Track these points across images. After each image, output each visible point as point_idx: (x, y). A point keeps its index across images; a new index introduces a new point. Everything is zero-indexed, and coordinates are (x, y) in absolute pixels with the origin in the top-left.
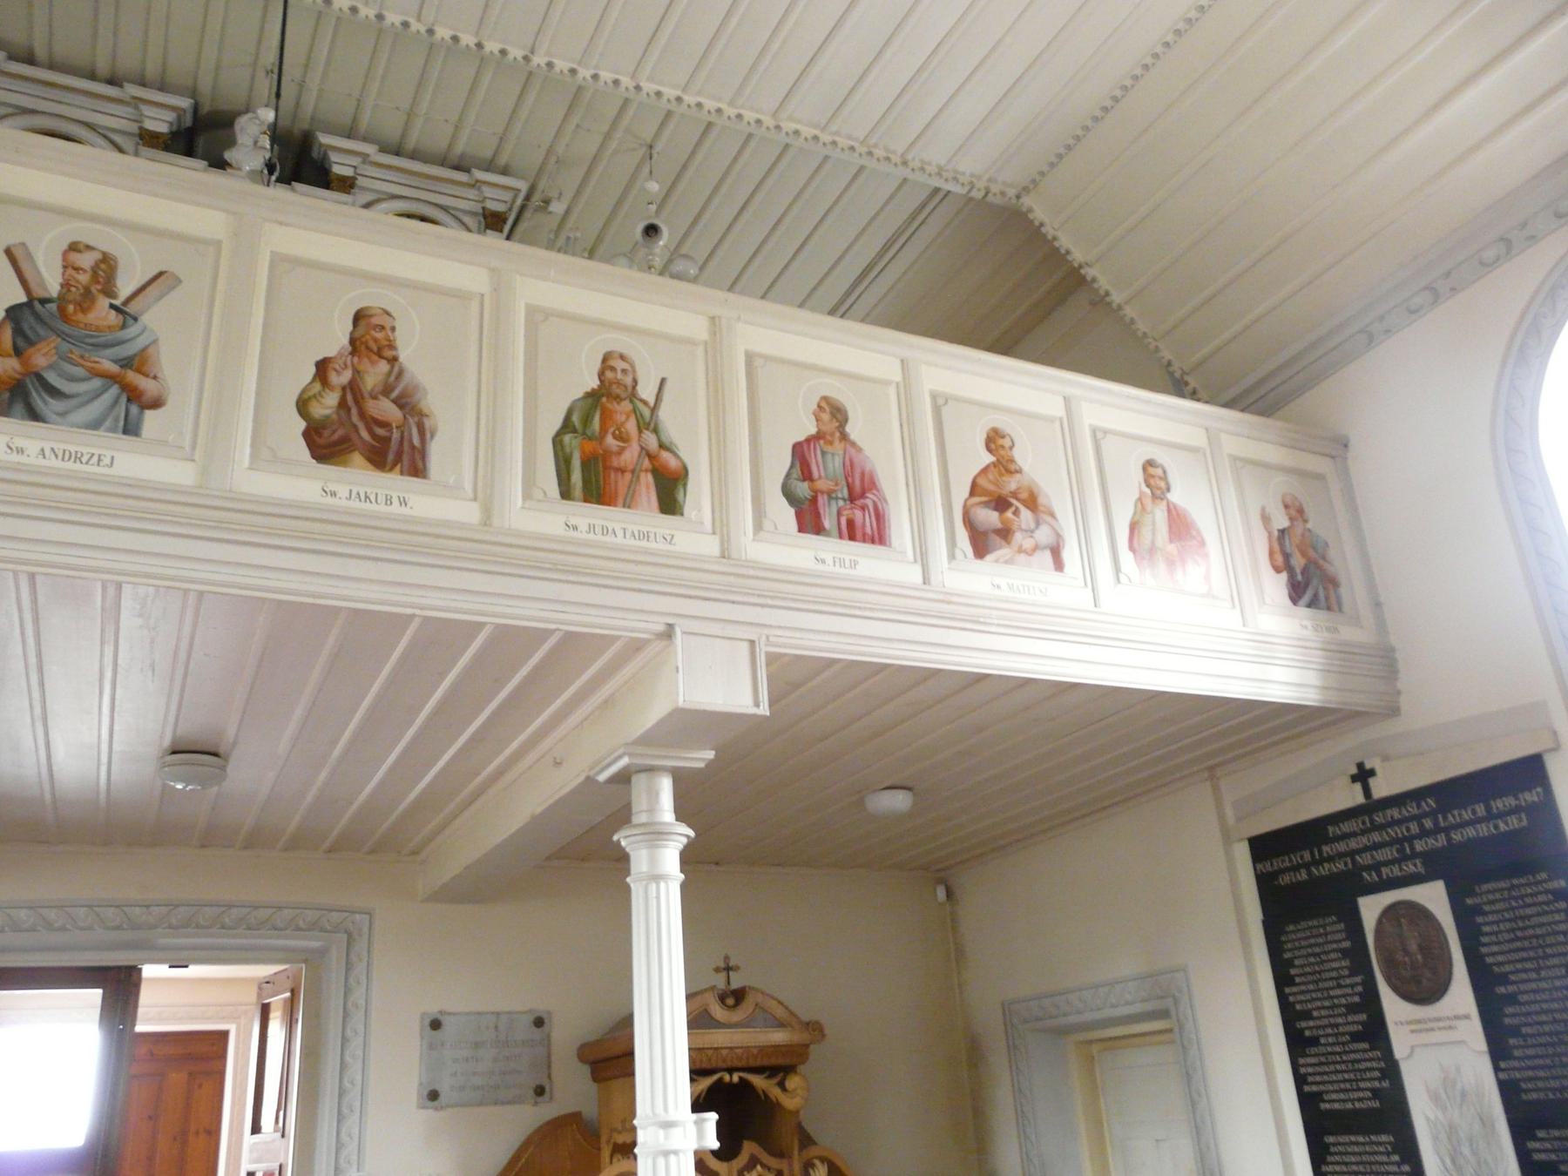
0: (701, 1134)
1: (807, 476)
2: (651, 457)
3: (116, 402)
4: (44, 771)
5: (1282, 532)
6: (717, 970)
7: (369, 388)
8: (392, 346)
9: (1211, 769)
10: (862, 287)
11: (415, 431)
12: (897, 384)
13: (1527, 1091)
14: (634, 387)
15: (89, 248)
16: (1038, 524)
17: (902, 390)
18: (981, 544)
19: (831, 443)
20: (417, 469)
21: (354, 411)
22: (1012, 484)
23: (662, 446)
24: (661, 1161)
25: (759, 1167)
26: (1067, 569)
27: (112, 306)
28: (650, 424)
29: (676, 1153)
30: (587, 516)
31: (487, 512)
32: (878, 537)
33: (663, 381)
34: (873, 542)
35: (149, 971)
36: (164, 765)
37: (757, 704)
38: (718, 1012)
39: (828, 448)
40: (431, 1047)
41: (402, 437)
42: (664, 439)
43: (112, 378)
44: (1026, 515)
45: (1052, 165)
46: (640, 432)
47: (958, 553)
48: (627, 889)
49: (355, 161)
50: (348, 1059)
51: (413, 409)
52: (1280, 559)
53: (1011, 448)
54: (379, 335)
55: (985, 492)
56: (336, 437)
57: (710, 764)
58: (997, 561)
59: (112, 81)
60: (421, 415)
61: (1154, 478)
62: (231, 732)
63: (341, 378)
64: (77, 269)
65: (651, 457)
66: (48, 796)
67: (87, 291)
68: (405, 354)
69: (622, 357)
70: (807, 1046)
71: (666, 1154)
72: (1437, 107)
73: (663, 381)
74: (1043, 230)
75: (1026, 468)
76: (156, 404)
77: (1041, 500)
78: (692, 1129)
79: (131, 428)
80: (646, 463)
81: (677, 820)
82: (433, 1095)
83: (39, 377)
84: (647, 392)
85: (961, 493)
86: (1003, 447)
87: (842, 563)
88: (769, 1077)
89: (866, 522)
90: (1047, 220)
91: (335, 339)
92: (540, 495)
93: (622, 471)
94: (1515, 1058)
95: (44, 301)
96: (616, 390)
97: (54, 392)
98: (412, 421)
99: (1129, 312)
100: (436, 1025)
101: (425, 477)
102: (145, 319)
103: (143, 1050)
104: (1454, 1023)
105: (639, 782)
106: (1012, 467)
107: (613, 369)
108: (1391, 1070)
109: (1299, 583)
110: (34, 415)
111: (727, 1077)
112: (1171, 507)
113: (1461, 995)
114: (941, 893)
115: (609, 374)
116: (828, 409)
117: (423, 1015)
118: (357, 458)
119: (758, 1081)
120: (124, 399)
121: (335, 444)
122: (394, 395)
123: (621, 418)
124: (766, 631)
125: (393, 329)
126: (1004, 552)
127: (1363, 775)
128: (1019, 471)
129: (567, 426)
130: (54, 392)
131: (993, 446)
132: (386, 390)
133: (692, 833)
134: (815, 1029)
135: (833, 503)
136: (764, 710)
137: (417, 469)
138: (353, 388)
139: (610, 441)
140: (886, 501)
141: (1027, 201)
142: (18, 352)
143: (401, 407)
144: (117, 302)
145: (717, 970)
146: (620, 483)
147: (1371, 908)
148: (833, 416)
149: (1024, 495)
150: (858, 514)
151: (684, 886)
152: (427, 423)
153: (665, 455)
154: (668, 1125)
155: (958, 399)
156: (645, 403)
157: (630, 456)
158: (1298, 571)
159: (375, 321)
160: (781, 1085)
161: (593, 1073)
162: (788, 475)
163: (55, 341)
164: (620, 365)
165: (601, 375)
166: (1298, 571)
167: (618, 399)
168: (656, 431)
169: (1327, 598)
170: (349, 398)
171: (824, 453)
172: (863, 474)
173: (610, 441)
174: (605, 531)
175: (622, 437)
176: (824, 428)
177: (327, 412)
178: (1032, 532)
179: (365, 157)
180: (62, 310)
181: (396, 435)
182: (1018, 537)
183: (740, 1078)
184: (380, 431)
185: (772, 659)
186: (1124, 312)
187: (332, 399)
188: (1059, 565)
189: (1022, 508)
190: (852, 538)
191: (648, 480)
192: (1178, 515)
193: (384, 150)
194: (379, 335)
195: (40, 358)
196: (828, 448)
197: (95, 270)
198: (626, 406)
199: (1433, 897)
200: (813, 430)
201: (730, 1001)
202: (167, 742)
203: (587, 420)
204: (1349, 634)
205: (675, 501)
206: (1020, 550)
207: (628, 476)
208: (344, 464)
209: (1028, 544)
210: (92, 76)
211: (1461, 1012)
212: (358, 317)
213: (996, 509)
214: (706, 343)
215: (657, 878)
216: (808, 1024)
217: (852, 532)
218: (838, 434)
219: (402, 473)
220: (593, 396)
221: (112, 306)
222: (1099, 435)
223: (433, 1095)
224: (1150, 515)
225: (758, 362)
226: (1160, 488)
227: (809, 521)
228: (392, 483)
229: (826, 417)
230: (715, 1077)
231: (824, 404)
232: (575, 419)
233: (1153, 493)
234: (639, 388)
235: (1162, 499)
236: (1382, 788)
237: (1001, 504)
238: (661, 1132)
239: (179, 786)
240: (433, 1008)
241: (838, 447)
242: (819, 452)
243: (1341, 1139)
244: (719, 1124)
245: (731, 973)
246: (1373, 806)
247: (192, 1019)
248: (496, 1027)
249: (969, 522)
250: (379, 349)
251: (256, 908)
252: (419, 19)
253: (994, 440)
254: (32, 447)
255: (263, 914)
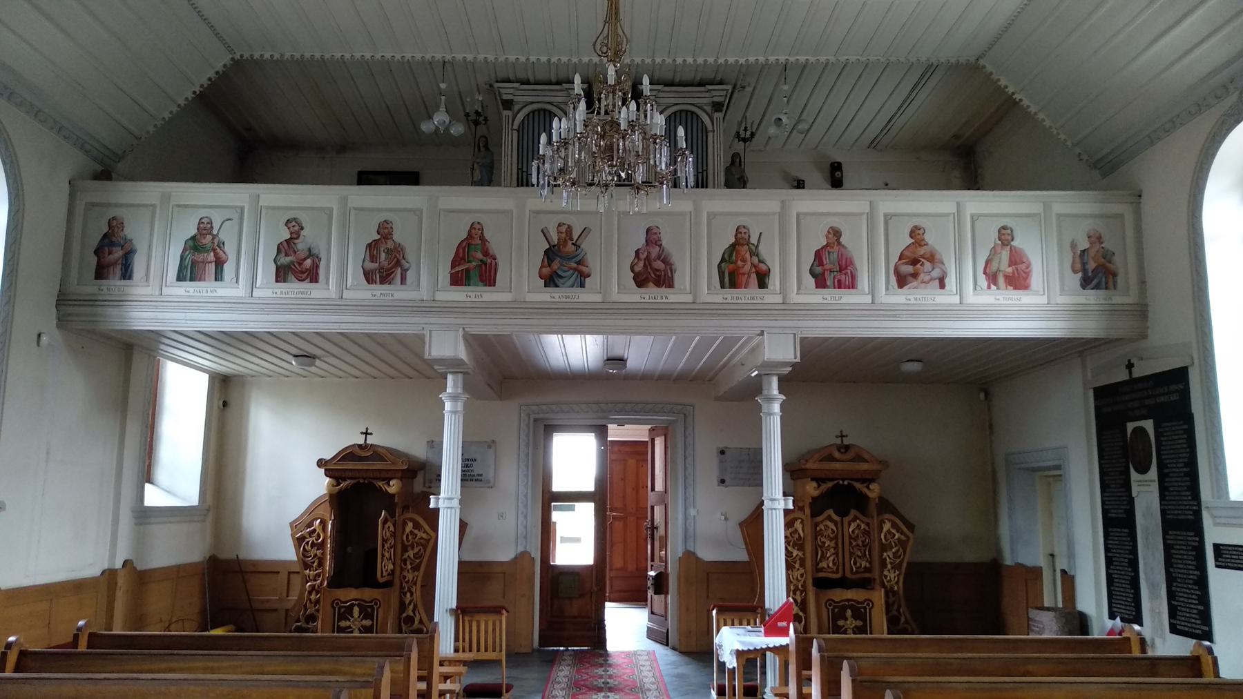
0: (786, 504)
1: (821, 264)
2: (755, 267)
3: (577, 276)
4: (567, 365)
5: (1083, 252)
6: (837, 437)
7: (653, 257)
8: (660, 240)
9: (1081, 352)
10: (917, 90)
11: (669, 271)
12: (867, 214)
13: (1169, 514)
14: (749, 239)
15: (564, 224)
16: (933, 269)
17: (869, 217)
18: (902, 281)
19: (833, 248)
20: (671, 286)
21: (649, 267)
22: (922, 251)
23: (760, 261)
24: (770, 511)
25: (858, 521)
26: (947, 287)
27: (573, 244)
28: (755, 253)
29: (775, 509)
30: (731, 295)
31: (695, 297)
32: (852, 285)
33: (761, 233)
34: (849, 288)
35: (609, 425)
36: (605, 365)
37: (795, 358)
38: (837, 455)
39: (832, 250)
40: (721, 462)
41: (665, 275)
42: (761, 258)
43: (575, 269)
44: (928, 265)
45: (989, 48)
46: (751, 257)
47: (890, 287)
48: (781, 411)
49: (511, 91)
50: (688, 465)
51: (668, 262)
52: (1078, 266)
53: (923, 234)
54: (655, 237)
55: (907, 258)
56: (643, 278)
57: (790, 372)
58: (909, 288)
59: (558, 83)
60: (671, 264)
61: (1005, 236)
62: (626, 357)
63: (643, 256)
64: (561, 233)
65: (755, 267)
66: (568, 370)
67: (565, 239)
68: (664, 243)
69: (744, 227)
70: (880, 471)
71: (772, 509)
72: (1155, 40)
73: (761, 233)
74: (992, 77)
75: (930, 242)
76: (589, 276)
77: (937, 256)
78: (782, 502)
79: (582, 285)
80: (754, 270)
81: (780, 393)
82: (723, 481)
83: (555, 272)
84: (754, 240)
85: (894, 259)
86: (919, 234)
87: (835, 299)
88: (862, 483)
89: (845, 279)
90: (994, 71)
91: (640, 241)
92: (713, 288)
93: (744, 274)
94: (1166, 500)
95: (554, 246)
96: (742, 241)
97: (561, 277)
98: (668, 268)
99: (1041, 116)
100: (722, 452)
101: (673, 287)
102: (582, 246)
103: (616, 448)
104: (1150, 483)
105: (765, 379)
106: (923, 243)
107: (475, 229)
108: (1131, 501)
109: (1089, 277)
110: (557, 286)
111: (841, 482)
112: (1013, 248)
113: (1153, 473)
114: (982, 396)
115: (739, 235)
116: (832, 233)
117: (718, 448)
118: (651, 284)
119: (857, 485)
120: (579, 276)
121: (643, 280)
122: (662, 258)
123: (743, 253)
124: (801, 329)
125: (660, 233)
126: (915, 284)
127: (1130, 366)
128: (927, 244)
129: (723, 260)
130: (561, 277)
131: (913, 235)
132: (659, 257)
133: (784, 398)
134: (885, 464)
135: (832, 274)
136: (798, 360)
137: (671, 286)
138: (648, 258)
139: (739, 263)
140: (856, 269)
141: (982, 62)
142: (549, 266)
143: (664, 263)
144: (574, 242)
145: (837, 437)
146: (743, 279)
147: (1130, 426)
148: (834, 235)
149: (928, 256)
150: (843, 277)
151: (781, 417)
152: (673, 267)
153: (761, 265)
154: (773, 500)
155: (896, 215)
156: (753, 244)
157: (748, 267)
158: (1090, 271)
159: (654, 231)
160: (868, 487)
161: (791, 476)
162: (812, 265)
163: (559, 259)
164: (743, 230)
165: (736, 236)
166: (1090, 271)
167: (743, 245)
168: (757, 256)
169: (1106, 283)
170: (647, 262)
171: (829, 252)
172: (847, 259)
173: (739, 263)
174: (737, 298)
175: (744, 261)
176: (830, 241)
177: (640, 269)
178: (930, 272)
179: (659, 91)
180: (559, 248)
181: (663, 273)
182: (922, 276)
183: (849, 483)
184: (658, 273)
185: (802, 339)
186: (1038, 116)
187: (641, 264)
188: (942, 286)
189: (925, 261)
190: (840, 287)
191: (754, 276)
192: (1016, 252)
193: (666, 85)
194: (655, 237)
195: (555, 266)
196: (832, 250)
197: (566, 231)
198: (746, 247)
199: (1148, 425)
200: (825, 243)
201: (843, 450)
202: (605, 358)
203: (730, 256)
204: (1118, 300)
205: (765, 283)
206: (923, 282)
207: (746, 276)
208: (647, 287)
209: (927, 278)
210: (550, 83)
211: (1153, 478)
212: (648, 231)
213: (911, 265)
214: (779, 213)
215: (770, 414)
216: (880, 462)
217: (840, 286)
218: (836, 243)
219: (666, 287)
220: (733, 246)
221: (573, 244)
222: (975, 218)
223: (723, 481)
224: (999, 255)
225: (802, 217)
226: (1007, 240)
227: (821, 283)
228: (663, 290)
229: (831, 236)
230: (836, 482)
231: (831, 231)
232: (726, 256)
233: (1002, 243)
234: (751, 239)
235: (1007, 245)
236: (1137, 373)
237: (915, 262)
238: (770, 502)
239: (611, 371)
240: (722, 446)
241: (836, 248)
242: (827, 253)
243: (1115, 530)
244: (430, 504)
245: (844, 439)
246: (1132, 381)
247: (635, 436)
248: (749, 454)
249: (897, 272)
250: (656, 242)
251: (647, 404)
252: (669, 57)
253: (915, 232)
254: (557, 295)
255: (650, 406)
